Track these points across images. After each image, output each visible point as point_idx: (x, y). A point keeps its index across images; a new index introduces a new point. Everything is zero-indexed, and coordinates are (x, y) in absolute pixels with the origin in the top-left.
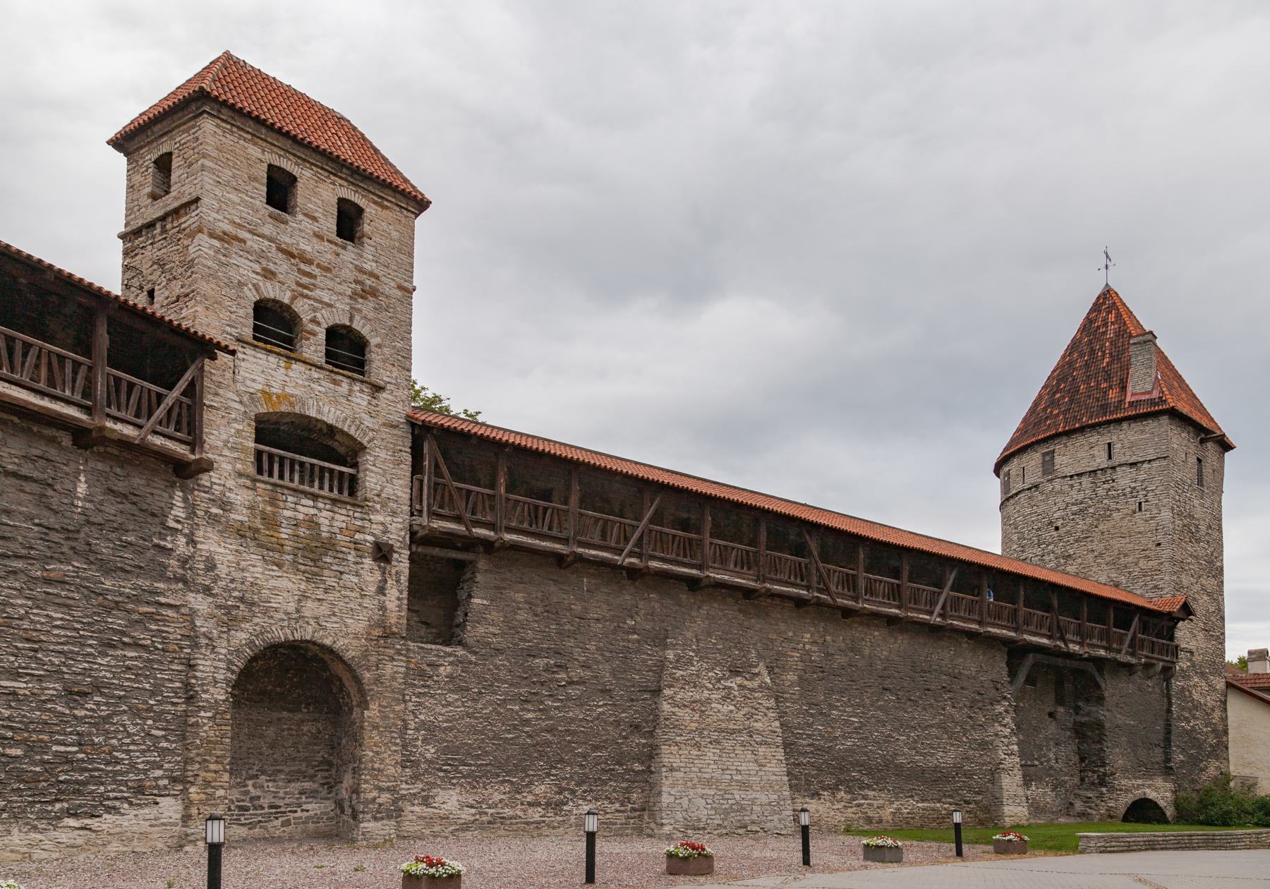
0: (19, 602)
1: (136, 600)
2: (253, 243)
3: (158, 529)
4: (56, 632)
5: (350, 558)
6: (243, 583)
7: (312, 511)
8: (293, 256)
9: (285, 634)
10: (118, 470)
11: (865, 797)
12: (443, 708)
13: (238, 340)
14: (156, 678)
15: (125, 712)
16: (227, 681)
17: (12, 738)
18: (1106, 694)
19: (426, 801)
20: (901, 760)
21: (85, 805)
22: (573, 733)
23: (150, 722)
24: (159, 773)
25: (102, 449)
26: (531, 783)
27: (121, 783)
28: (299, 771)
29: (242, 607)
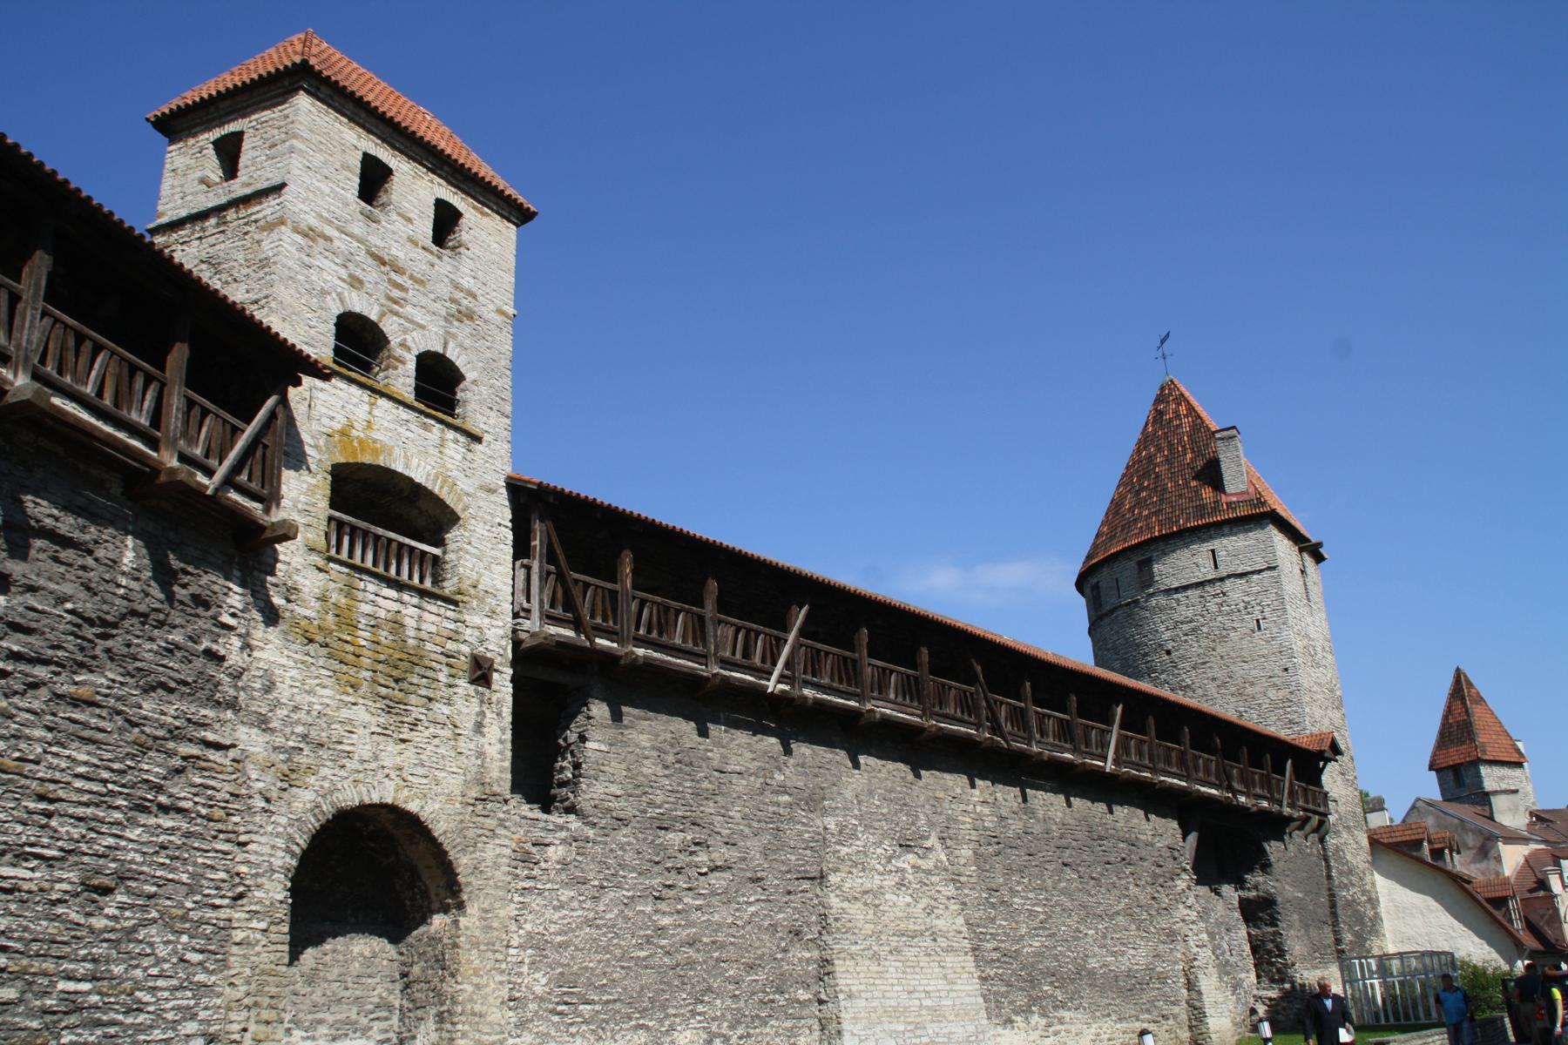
1: (174, 734)
2: (341, 243)
4: (79, 784)
5: (442, 677)
6: (309, 712)
9: (360, 793)
10: (171, 534)
11: (1061, 1021)
12: (554, 912)
14: (195, 864)
15: (155, 921)
18: (1272, 859)
20: (1093, 963)
22: (722, 946)
23: (185, 938)
26: (672, 1028)
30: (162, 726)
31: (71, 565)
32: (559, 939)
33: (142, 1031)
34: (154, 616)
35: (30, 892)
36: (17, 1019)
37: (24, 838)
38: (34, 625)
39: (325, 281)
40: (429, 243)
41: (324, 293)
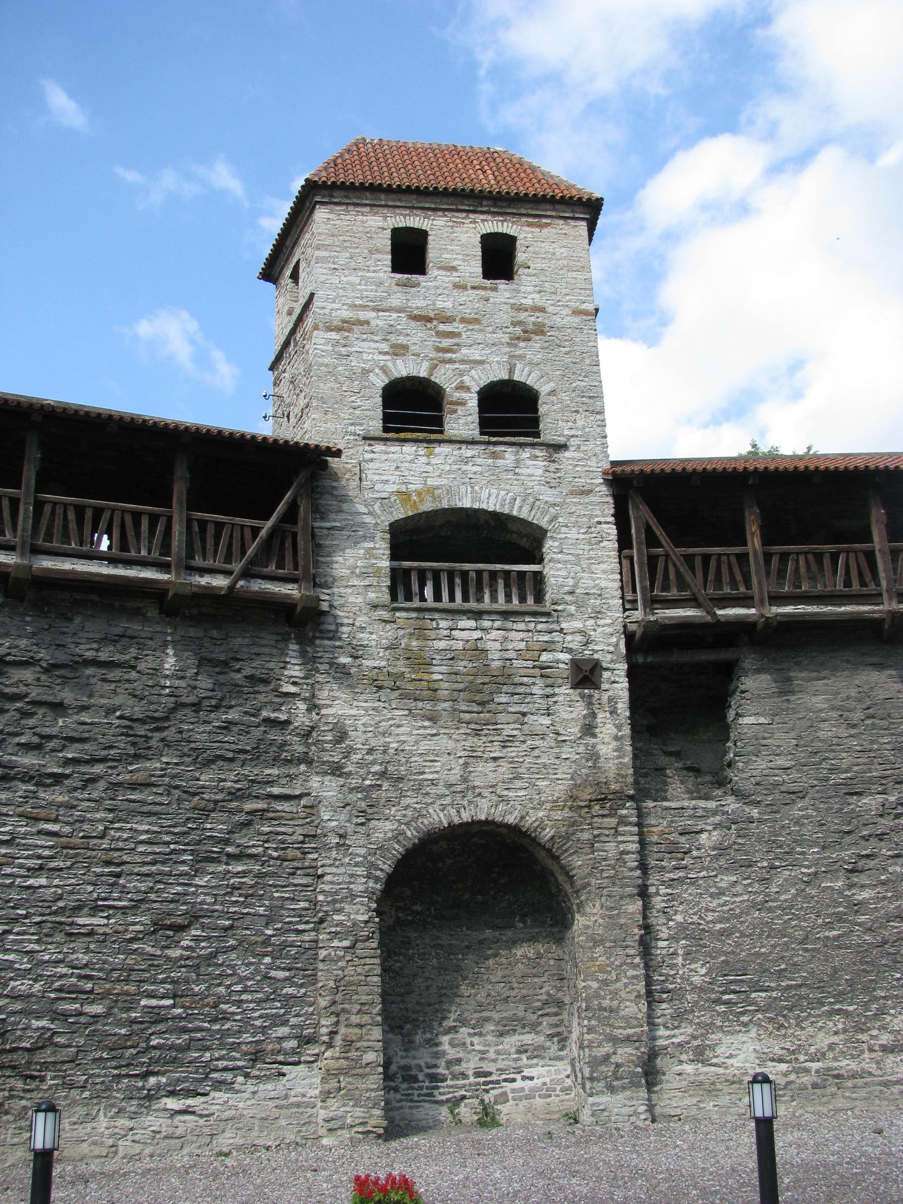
0: (98, 816)
2: (378, 321)
3: (271, 697)
4: (141, 849)
5: (536, 690)
6: (385, 752)
7: (477, 634)
8: (430, 320)
10: (215, 633)
13: (365, 438)
14: (272, 898)
15: (233, 948)
16: (369, 893)
17: (91, 992)
19: (700, 1055)
21: (185, 1079)
23: (267, 960)
24: (283, 1031)
25: (195, 612)
26: (882, 1011)
27: (235, 1047)
28: (514, 1019)
29: (386, 785)
30: (222, 790)
31: (119, 681)
32: (718, 926)
33: (230, 1036)
34: (206, 703)
35: (105, 934)
36: (107, 1028)
37: (95, 895)
38: (86, 735)
39: (366, 362)
40: (480, 280)
41: (366, 372)
